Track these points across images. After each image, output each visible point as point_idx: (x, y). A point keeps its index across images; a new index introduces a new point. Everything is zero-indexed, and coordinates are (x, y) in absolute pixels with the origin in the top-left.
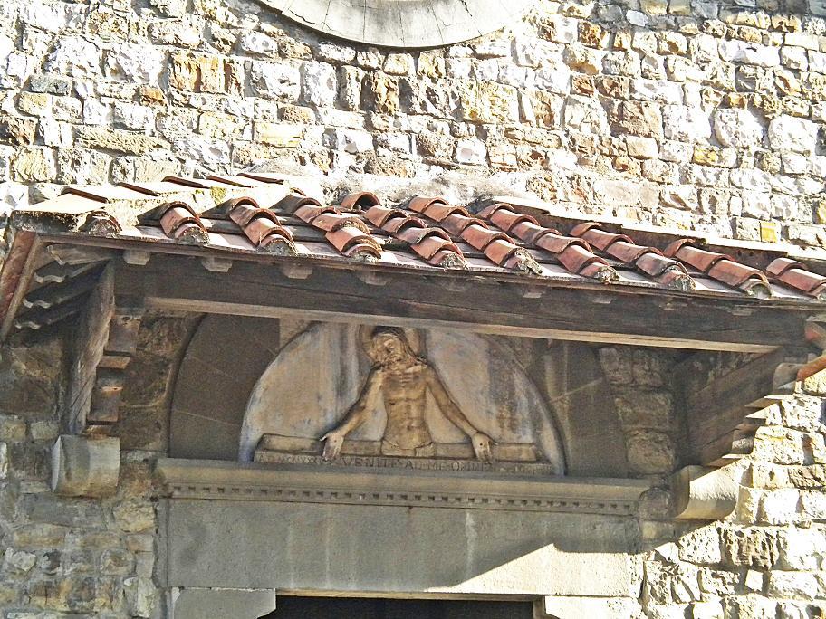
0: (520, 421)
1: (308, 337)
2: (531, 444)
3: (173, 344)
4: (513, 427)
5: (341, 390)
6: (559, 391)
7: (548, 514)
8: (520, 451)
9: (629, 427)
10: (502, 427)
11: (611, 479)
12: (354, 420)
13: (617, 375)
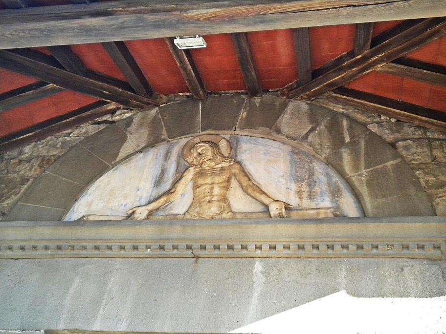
0: (319, 193)
1: (141, 155)
2: (329, 208)
3: (40, 169)
4: (311, 197)
5: (158, 182)
6: (356, 168)
7: (346, 260)
8: (318, 214)
9: (434, 191)
10: (301, 198)
11: (410, 218)
12: (162, 200)
13: (417, 157)
